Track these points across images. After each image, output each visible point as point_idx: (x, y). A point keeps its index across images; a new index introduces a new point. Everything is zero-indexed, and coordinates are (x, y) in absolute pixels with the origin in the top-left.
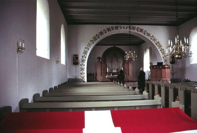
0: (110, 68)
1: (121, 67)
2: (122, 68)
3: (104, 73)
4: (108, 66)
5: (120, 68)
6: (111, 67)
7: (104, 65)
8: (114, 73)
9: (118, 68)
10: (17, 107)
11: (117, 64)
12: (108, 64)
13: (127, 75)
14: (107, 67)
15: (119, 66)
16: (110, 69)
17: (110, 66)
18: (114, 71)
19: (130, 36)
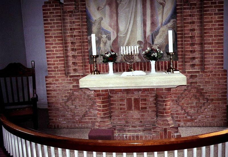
0: (106, 32)
1: (164, 28)
2: (170, 33)
3: (79, 60)
4: (100, 23)
5: (157, 33)
6: (110, 30)
7: (74, 19)
8: (130, 57)
9: (148, 33)
10: (155, 38)
11: (144, 14)
12: (95, 15)
13: (197, 69)
14: (95, 28)
15: (153, 24)
16: (109, 39)
17: (106, 24)
18: (125, 51)
19: (132, 106)
